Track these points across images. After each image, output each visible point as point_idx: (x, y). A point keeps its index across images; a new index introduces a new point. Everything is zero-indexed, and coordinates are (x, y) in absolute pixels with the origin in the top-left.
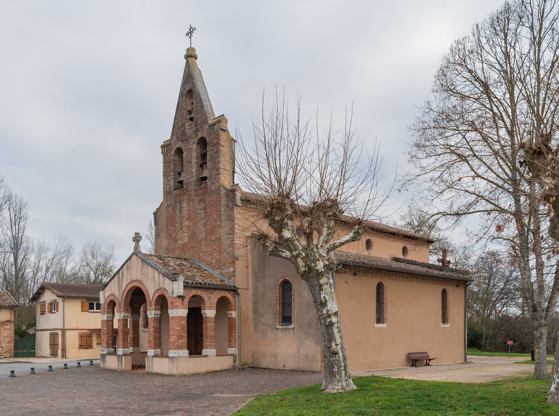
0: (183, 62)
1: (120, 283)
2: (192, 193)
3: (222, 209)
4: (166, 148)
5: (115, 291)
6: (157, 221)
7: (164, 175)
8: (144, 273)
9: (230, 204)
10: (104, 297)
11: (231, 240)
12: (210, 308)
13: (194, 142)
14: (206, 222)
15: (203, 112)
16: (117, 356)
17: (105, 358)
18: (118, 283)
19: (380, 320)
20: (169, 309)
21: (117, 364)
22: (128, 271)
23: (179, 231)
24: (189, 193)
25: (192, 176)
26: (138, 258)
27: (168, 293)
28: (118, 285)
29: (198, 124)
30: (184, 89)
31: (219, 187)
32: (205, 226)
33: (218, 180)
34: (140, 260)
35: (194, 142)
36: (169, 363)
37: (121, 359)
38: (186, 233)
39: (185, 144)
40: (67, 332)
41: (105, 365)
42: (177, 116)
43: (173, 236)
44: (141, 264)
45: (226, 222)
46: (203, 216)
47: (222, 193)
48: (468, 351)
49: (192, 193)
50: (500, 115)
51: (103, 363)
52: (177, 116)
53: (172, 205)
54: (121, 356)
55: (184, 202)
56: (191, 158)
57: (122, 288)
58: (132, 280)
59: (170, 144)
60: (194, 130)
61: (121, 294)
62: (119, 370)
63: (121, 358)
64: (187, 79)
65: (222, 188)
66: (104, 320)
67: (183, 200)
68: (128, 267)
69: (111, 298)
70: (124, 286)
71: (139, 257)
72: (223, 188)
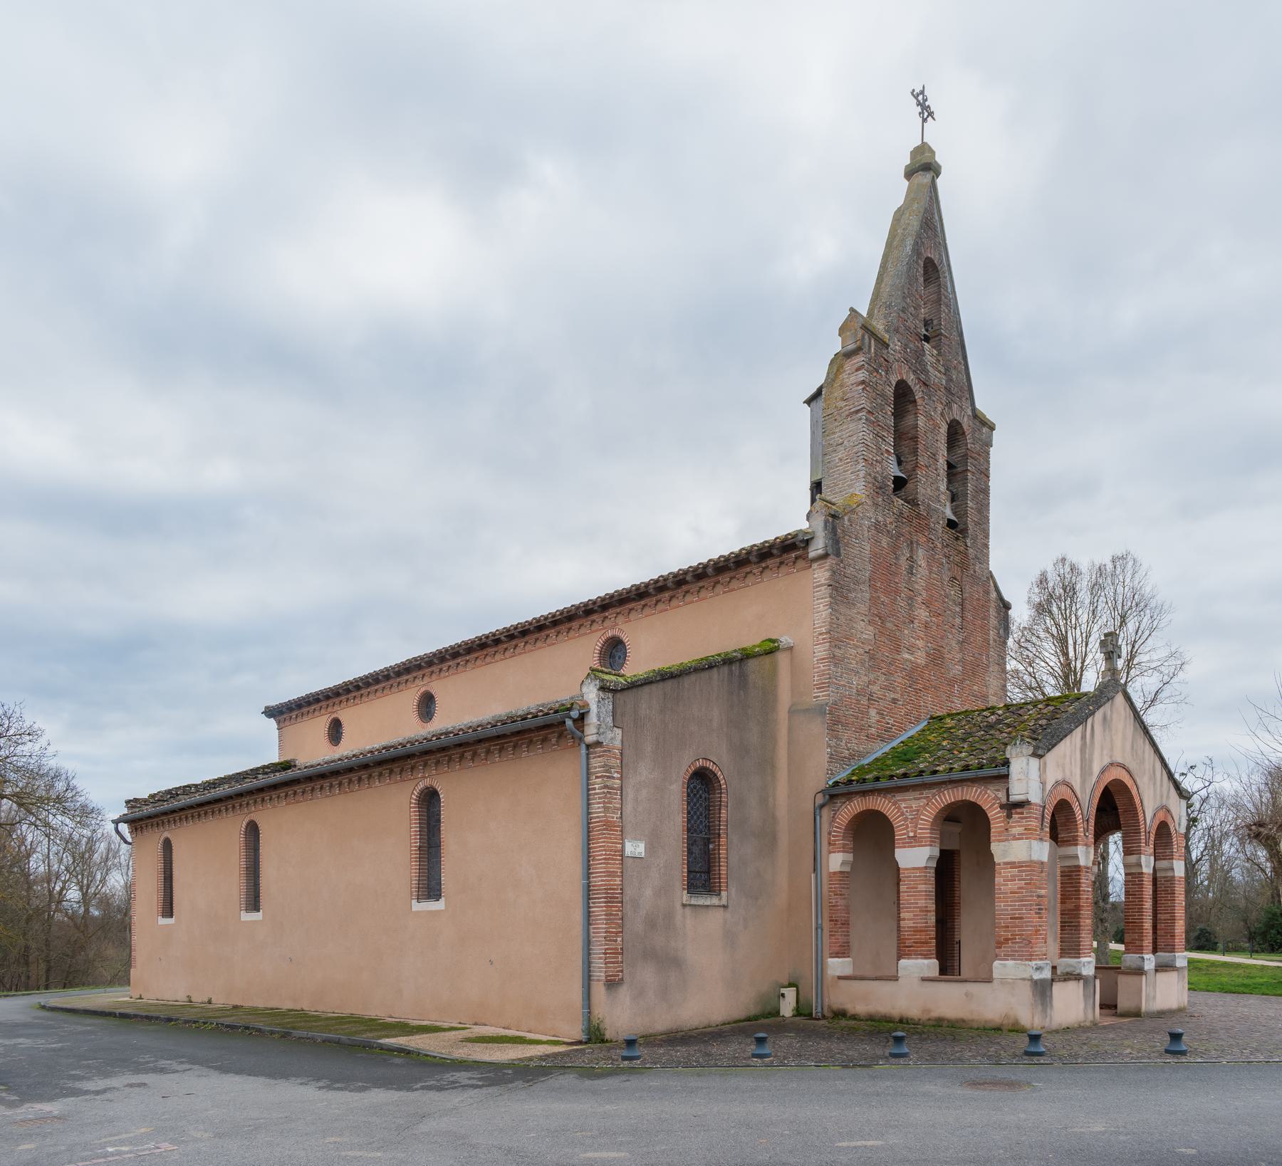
0: (897, 191)
1: (1087, 756)
10: (1043, 783)
12: (915, 841)
16: (1082, 982)
17: (1048, 994)
18: (1081, 750)
19: (430, 888)
20: (994, 841)
21: (1082, 1006)
22: (1104, 730)
28: (1082, 760)
36: (1178, 974)
37: (1092, 990)
41: (1048, 1020)
48: (122, 978)
50: (1064, 633)
51: (1044, 1011)
54: (1092, 981)
57: (1091, 774)
61: (1088, 791)
62: (1088, 1024)
63: (1092, 984)
66: (1042, 863)
68: (1105, 718)
69: (1065, 793)
70: (1096, 769)
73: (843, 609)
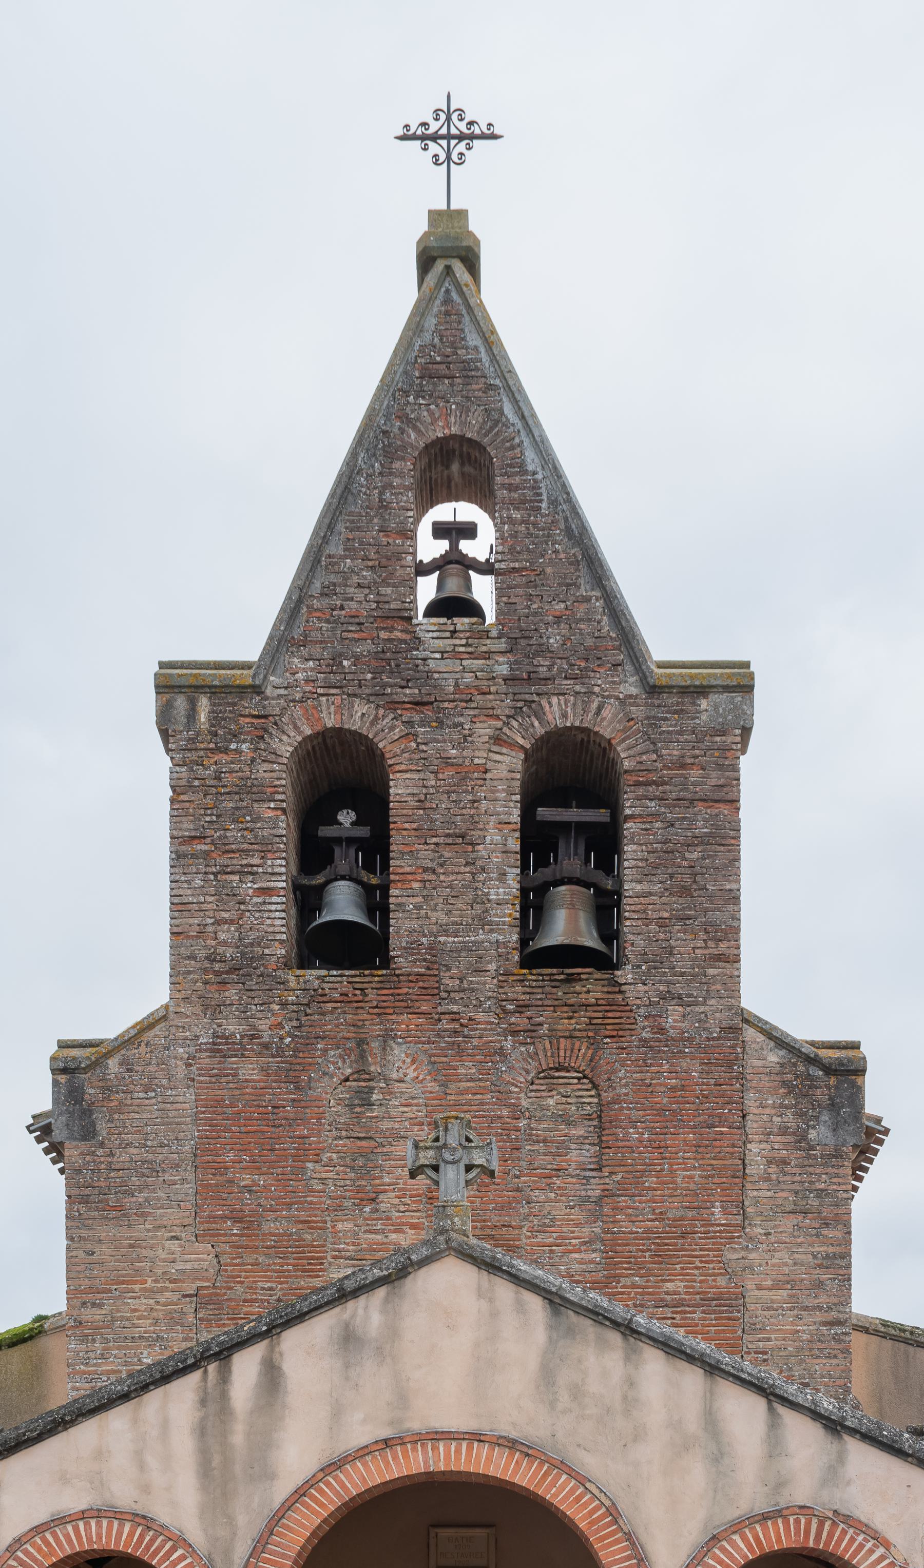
2: (480, 1016)
3: (754, 1148)
4: (204, 703)
5: (146, 1489)
6: (87, 1113)
7: (179, 858)
8: (577, 1393)
9: (819, 1134)
11: (819, 1316)
13: (498, 740)
14: (607, 1194)
15: (587, 600)
22: (347, 1366)
23: (339, 1208)
24: (455, 1008)
25: (483, 921)
26: (504, 1290)
27: (887, 1545)
29: (543, 650)
30: (403, 417)
31: (733, 1031)
32: (595, 1217)
33: (733, 990)
34: (535, 1303)
35: (498, 740)
38: (413, 1226)
39: (409, 723)
40: (453, 207)
42: (335, 548)
43: (269, 1226)
44: (540, 1335)
45: (788, 1223)
46: (580, 1155)
47: (759, 1063)
49: (480, 1016)
52: (335, 548)
53: (266, 1046)
55: (398, 1052)
56: (473, 822)
58: (416, 1425)
59: (257, 690)
60: (503, 670)
64: (428, 374)
65: (750, 1033)
67: (387, 1037)
71: (516, 1279)
72: (761, 1038)
73: (103, 1232)
